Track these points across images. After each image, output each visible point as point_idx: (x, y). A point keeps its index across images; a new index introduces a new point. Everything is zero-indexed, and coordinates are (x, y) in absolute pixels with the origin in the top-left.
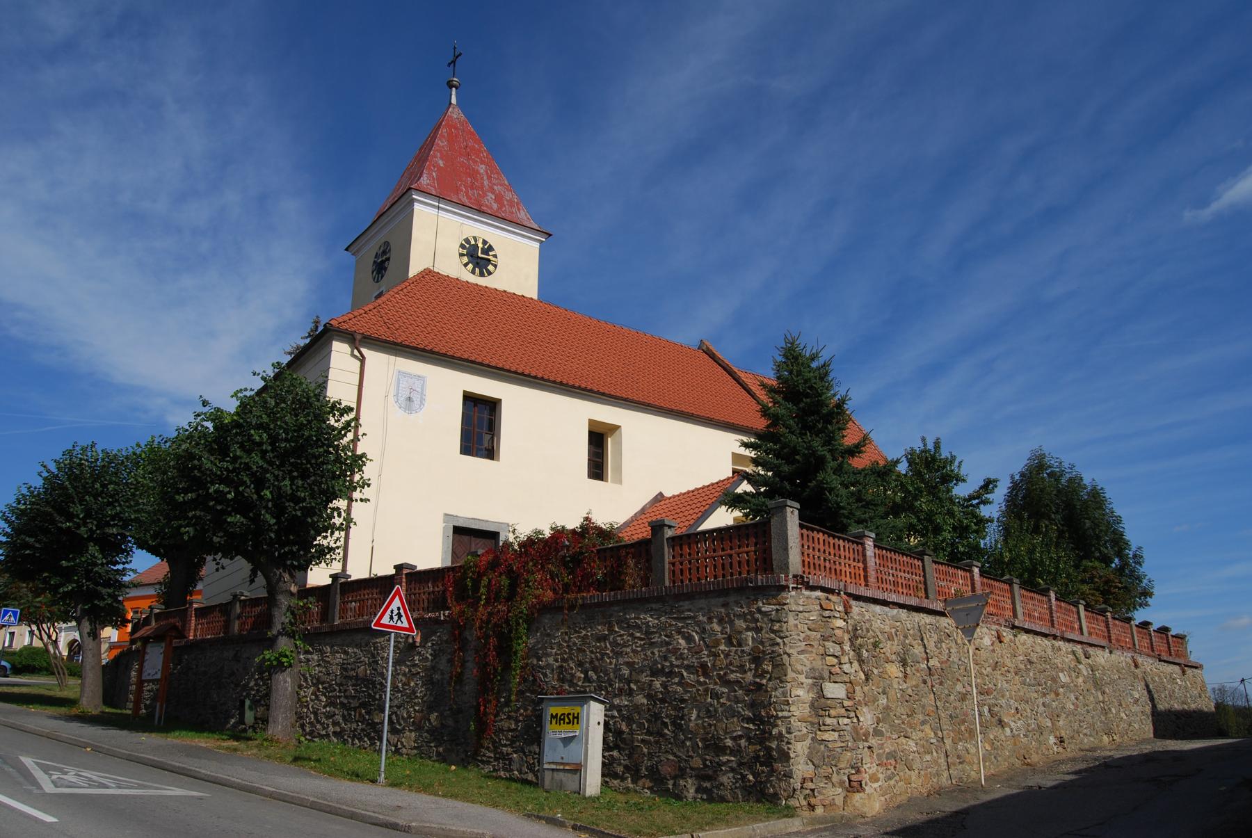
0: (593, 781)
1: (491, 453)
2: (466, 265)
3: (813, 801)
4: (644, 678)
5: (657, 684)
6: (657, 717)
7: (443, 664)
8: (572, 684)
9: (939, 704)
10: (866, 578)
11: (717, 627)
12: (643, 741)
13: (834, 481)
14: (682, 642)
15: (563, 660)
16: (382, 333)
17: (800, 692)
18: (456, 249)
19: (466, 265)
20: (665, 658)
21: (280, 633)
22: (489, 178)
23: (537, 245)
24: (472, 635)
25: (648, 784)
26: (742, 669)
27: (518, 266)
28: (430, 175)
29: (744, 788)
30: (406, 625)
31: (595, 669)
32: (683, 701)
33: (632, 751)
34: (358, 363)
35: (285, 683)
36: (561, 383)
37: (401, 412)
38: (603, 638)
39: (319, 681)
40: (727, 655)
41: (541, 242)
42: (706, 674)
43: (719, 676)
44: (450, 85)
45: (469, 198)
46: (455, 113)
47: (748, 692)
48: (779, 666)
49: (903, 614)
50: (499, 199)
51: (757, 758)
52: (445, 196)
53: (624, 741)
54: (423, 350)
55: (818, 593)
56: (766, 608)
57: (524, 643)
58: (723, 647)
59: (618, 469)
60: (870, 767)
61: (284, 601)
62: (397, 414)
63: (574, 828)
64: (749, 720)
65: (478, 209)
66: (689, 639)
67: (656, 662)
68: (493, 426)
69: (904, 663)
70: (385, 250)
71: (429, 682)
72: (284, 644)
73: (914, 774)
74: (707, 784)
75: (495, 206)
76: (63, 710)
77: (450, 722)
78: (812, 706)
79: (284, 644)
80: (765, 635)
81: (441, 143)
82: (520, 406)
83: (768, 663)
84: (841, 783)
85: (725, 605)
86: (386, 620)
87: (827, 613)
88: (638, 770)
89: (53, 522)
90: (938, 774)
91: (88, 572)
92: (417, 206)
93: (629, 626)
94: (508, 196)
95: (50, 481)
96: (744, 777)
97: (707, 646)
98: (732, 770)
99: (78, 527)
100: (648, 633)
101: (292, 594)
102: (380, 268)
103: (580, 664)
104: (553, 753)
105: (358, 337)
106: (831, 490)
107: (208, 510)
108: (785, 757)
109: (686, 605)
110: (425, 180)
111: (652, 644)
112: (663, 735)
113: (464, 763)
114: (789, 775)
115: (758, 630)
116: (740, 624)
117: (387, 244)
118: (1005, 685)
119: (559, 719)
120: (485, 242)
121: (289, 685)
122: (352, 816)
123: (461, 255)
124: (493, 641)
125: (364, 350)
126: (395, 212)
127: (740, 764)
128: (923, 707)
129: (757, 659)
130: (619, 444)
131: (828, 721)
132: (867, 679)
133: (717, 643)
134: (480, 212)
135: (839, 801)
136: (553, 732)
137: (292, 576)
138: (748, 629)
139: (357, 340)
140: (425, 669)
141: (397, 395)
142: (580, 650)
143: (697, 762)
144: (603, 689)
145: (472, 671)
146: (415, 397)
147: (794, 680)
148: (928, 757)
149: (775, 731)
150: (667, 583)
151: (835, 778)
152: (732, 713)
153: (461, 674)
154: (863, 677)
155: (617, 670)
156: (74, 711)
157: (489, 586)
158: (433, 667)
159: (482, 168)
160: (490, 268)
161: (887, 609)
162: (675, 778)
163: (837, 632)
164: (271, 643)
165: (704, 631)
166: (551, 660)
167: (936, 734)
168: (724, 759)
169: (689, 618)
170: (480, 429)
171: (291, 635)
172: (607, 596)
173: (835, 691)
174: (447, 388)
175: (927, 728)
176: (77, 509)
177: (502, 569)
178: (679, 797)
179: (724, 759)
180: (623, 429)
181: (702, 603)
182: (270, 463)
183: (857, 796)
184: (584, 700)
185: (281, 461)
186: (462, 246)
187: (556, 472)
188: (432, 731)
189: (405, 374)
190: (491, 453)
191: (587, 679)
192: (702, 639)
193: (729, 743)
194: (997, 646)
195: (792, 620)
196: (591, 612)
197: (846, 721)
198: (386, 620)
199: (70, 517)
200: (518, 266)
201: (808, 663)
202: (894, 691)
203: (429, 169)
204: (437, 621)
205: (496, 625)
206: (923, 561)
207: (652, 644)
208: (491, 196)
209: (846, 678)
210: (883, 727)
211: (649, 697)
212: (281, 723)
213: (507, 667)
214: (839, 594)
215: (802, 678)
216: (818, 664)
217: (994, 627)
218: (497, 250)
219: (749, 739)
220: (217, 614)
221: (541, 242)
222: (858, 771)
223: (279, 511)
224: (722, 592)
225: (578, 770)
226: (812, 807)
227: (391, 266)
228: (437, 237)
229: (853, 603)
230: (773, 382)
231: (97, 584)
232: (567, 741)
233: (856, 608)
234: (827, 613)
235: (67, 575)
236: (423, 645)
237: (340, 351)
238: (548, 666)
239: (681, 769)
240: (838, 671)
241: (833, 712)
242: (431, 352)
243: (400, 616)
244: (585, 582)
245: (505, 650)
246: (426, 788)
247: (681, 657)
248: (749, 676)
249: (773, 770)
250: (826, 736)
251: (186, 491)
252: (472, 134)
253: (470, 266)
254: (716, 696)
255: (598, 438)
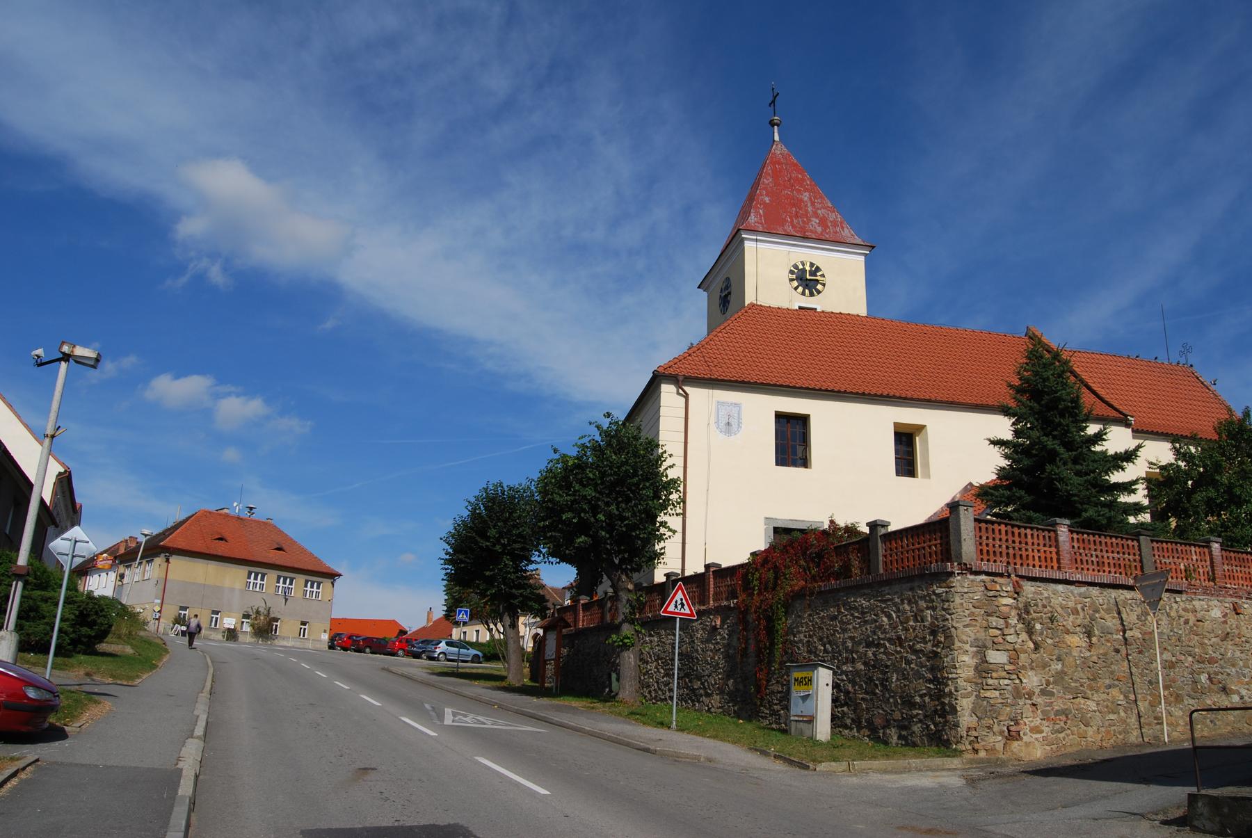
0: (823, 729)
1: (805, 462)
2: (796, 289)
3: (976, 746)
4: (862, 649)
5: (870, 654)
6: (871, 679)
7: (735, 643)
8: (817, 655)
9: (1134, 670)
10: (1058, 561)
11: (907, 607)
12: (862, 699)
13: (1067, 472)
14: (885, 619)
15: (810, 636)
16: (702, 372)
17: (966, 658)
18: (786, 276)
19: (796, 289)
20: (874, 633)
21: (623, 621)
22: (813, 204)
23: (862, 258)
24: (751, 617)
25: (867, 733)
26: (924, 641)
27: (845, 284)
28: (757, 213)
29: (928, 735)
30: (688, 611)
31: (830, 643)
32: (887, 667)
33: (856, 708)
34: (683, 400)
35: (629, 659)
36: (863, 394)
37: (722, 436)
38: (834, 618)
39: (659, 658)
40: (914, 630)
41: (866, 255)
42: (901, 645)
43: (910, 647)
44: (772, 124)
45: (794, 227)
46: (779, 150)
47: (929, 659)
48: (949, 637)
49: (1095, 591)
50: (823, 222)
51: (936, 711)
52: (774, 229)
53: (850, 699)
54: (736, 381)
55: (983, 577)
56: (939, 591)
57: (783, 624)
58: (911, 623)
59: (926, 465)
60: (1031, 719)
61: (624, 596)
62: (719, 437)
63: (775, 757)
64: (930, 681)
65: (803, 236)
66: (889, 617)
67: (868, 637)
68: (805, 439)
69: (1089, 634)
70: (727, 285)
71: (727, 657)
72: (627, 630)
73: (1090, 731)
74: (904, 733)
75: (819, 229)
76: (498, 684)
77: (741, 687)
78: (976, 668)
79: (627, 630)
80: (940, 612)
81: (767, 181)
82: (829, 420)
83: (941, 634)
84: (1001, 733)
85: (911, 589)
86: (671, 608)
87: (992, 593)
88: (860, 723)
89: (476, 543)
90: (1126, 732)
91: (504, 579)
92: (747, 244)
93: (851, 608)
94: (832, 216)
95: (474, 515)
96: (928, 726)
97: (902, 623)
98: (920, 721)
99: (494, 545)
100: (863, 613)
101: (630, 591)
102: (725, 301)
103: (821, 639)
104: (797, 708)
105: (681, 378)
106: (1061, 480)
107: (560, 531)
108: (954, 710)
109: (886, 589)
110: (752, 219)
111: (866, 622)
112: (875, 694)
113: (749, 719)
114: (957, 725)
115: (934, 608)
116: (922, 604)
117: (728, 279)
118: (1238, 654)
119: (799, 681)
120: (812, 265)
121: (632, 660)
122: (628, 744)
123: (791, 280)
124: (763, 622)
125: (687, 389)
126: (732, 251)
127: (926, 716)
128: (1112, 673)
129: (934, 633)
130: (925, 442)
131: (990, 681)
132: (1036, 649)
133: (907, 620)
134: (805, 238)
135: (999, 746)
136: (797, 692)
137: (627, 575)
138: (928, 608)
139: (680, 381)
140: (724, 646)
141: (717, 422)
142: (820, 628)
143: (897, 716)
144: (834, 659)
145: (752, 648)
146: (734, 422)
147: (960, 648)
148: (1112, 717)
149: (947, 690)
150: (881, 571)
151: (996, 728)
152: (919, 676)
153: (746, 648)
154: (1032, 646)
155: (844, 643)
156: (504, 684)
157: (760, 579)
158: (729, 644)
159: (806, 196)
160: (819, 287)
161: (1072, 587)
162: (884, 728)
163: (1002, 608)
164: (616, 628)
165: (898, 610)
166: (802, 636)
167: (1126, 697)
168: (915, 712)
169: (889, 600)
170: (792, 443)
171: (632, 622)
172: (842, 583)
173: (997, 657)
174: (759, 412)
175: (1115, 692)
176: (628, 514)
177: (770, 565)
178: (886, 743)
179: (915, 712)
180: (928, 428)
181: (897, 588)
182: (601, 493)
183: (1015, 744)
184: (815, 666)
185: (616, 488)
186: (791, 272)
187: (872, 471)
188: (730, 694)
189: (723, 404)
190: (805, 462)
191: (826, 651)
192: (898, 617)
193: (918, 699)
194: (1232, 620)
195: (958, 600)
196: (828, 597)
197: (1007, 682)
198: (671, 608)
199: (487, 539)
200: (845, 284)
201: (972, 635)
202: (1054, 661)
203: (756, 207)
204: (728, 607)
205: (766, 610)
206: (1138, 541)
207: (866, 622)
208: (815, 221)
209: (1010, 647)
210: (1054, 689)
211: (865, 664)
212: (627, 689)
213: (772, 644)
214: (1009, 576)
215: (967, 647)
216: (982, 635)
217: (1229, 599)
218: (824, 271)
219: (931, 696)
220: (596, 608)
221: (866, 255)
222: (1017, 723)
223: (610, 527)
224: (909, 579)
225: (811, 720)
226: (976, 751)
227: (732, 298)
228: (768, 270)
229: (1023, 583)
230: (1016, 382)
231: (511, 588)
232: (805, 698)
233: (1029, 588)
234: (992, 593)
235: (490, 581)
236: (722, 627)
237: (668, 392)
238: (801, 641)
239: (888, 721)
240: (1000, 639)
241: (994, 675)
242: (743, 382)
243: (683, 605)
244: (827, 575)
245: (771, 631)
246: (701, 732)
247: (884, 632)
248: (929, 646)
249: (946, 722)
250: (988, 694)
251: (543, 519)
252: (795, 165)
253: (800, 289)
254: (908, 662)
255: (906, 439)
